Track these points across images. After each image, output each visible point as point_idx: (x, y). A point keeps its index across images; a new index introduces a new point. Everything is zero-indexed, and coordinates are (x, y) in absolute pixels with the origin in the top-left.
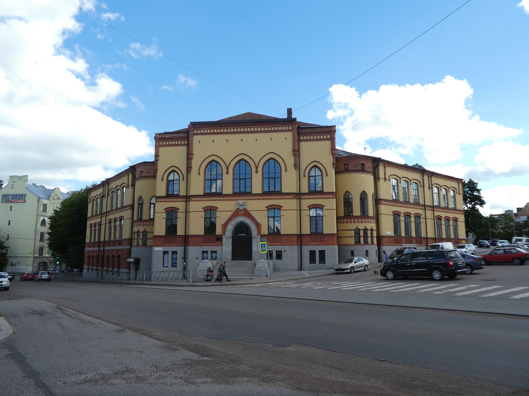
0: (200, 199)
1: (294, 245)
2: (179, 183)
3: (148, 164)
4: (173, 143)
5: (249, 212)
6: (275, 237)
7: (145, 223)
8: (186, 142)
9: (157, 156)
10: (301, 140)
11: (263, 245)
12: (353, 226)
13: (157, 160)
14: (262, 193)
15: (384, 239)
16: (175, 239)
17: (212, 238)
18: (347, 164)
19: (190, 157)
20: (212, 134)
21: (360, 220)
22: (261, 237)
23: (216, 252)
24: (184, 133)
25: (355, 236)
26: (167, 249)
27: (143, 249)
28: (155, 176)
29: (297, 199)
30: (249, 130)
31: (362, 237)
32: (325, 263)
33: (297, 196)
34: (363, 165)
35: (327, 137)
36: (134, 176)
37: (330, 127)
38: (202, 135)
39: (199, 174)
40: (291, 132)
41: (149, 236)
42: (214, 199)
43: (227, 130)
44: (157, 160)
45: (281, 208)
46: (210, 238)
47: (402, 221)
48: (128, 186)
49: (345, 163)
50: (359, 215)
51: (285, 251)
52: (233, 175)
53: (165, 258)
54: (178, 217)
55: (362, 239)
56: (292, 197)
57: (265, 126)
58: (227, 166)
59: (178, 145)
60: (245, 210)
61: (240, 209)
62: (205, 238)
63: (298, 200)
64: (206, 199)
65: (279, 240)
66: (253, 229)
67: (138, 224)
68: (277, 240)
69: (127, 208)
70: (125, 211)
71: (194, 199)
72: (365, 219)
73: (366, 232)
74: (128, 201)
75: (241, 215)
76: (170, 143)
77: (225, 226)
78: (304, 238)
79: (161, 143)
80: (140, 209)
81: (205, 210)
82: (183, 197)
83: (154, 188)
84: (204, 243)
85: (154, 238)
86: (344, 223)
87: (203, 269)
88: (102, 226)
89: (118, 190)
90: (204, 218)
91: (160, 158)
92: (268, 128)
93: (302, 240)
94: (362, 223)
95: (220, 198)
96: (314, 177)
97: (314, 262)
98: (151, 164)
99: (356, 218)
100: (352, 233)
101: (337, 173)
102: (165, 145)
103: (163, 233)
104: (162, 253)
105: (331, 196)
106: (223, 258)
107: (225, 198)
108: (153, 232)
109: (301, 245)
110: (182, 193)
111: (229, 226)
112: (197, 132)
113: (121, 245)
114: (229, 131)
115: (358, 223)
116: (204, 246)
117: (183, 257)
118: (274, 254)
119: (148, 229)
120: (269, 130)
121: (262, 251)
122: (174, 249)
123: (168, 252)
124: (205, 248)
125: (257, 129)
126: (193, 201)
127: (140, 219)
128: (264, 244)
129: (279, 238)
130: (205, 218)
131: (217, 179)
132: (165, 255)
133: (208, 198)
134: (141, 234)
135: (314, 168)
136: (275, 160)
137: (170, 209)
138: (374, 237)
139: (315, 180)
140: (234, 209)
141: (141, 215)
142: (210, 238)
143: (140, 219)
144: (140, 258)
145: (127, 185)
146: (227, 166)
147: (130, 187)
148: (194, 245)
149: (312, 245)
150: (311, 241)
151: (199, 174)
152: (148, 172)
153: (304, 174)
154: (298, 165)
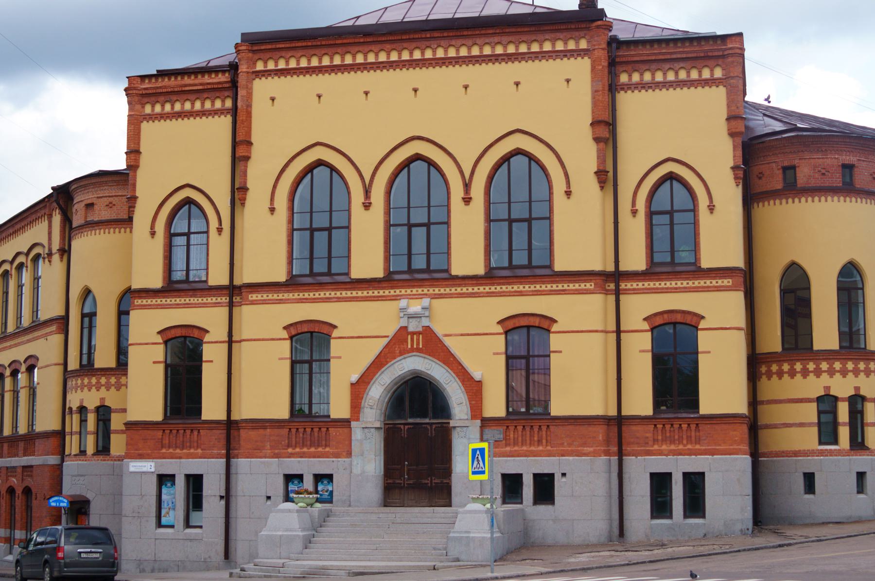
0: (275, 296)
1: (595, 454)
2: (208, 244)
3: (109, 178)
4: (188, 106)
5: (440, 341)
6: (532, 426)
7: (103, 380)
8: (229, 103)
9: (133, 152)
10: (623, 84)
11: (478, 452)
12: (814, 386)
13: (133, 168)
14: (486, 273)
15: (243, 433)
16: (196, 433)
17: (316, 430)
18: (793, 168)
19: (241, 152)
20: (314, 72)
21: (837, 365)
22: (482, 427)
23: (330, 477)
24: (224, 72)
25: (80, 432)
26: (168, 466)
27: (101, 465)
28: (128, 221)
29: (607, 292)
30: (440, 53)
31: (844, 424)
32: (703, 516)
33: (606, 281)
34: (848, 168)
35: (642, 79)
36: (67, 220)
37: (724, 38)
38: (282, 78)
39: (272, 210)
40: (586, 58)
41: (116, 422)
42: (322, 295)
43: (366, 58)
44: (133, 168)
45: (550, 326)
46: (309, 430)
47: (613, 332)
48: (50, 255)
49: (786, 164)
50: (836, 347)
51: (564, 475)
52: (388, 213)
53: (164, 497)
54: (552, 349)
55: (844, 433)
56: (588, 285)
57: (496, 39)
58: (367, 180)
59: (203, 113)
60: (428, 333)
61: (411, 329)
62: (294, 431)
63: (612, 298)
64: (296, 296)
65: (544, 436)
66: (453, 399)
67: (79, 382)
68: (536, 439)
69: (48, 330)
70: (42, 340)
71: (254, 297)
72: (804, 361)
73: (859, 407)
74: (50, 308)
75: (412, 350)
76: (178, 107)
77: (359, 389)
78: (629, 431)
79: (148, 109)
80: (86, 331)
81: (293, 333)
82: (218, 290)
83: (127, 265)
84: (289, 446)
85: (126, 430)
86: (780, 374)
87: (280, 533)
88: (28, 385)
89: (21, 266)
90: (503, 357)
91: (144, 160)
92: (505, 47)
93: (624, 435)
94: (844, 377)
95: (344, 293)
96: (668, 216)
97: (668, 514)
98: (115, 178)
99: (824, 360)
100: (810, 413)
101: (750, 200)
102: (149, 115)
103: (157, 415)
104: (154, 480)
105: (726, 281)
106: (352, 499)
107: (360, 294)
108: (124, 411)
109: (621, 454)
110: (218, 277)
111: (372, 389)
112: (276, 65)
113: (33, 454)
114: (371, 58)
115: (831, 377)
116: (290, 456)
117: (223, 494)
118: (528, 490)
119: (111, 399)
120: (346, 65)
121: (474, 473)
122: (194, 466)
123: (172, 478)
124: (294, 465)
125: (366, 59)
126: (253, 303)
127: (88, 368)
128: (482, 450)
129: (544, 428)
130: (293, 363)
131: (192, 230)
132: (163, 487)
133: (301, 294)
134: (91, 418)
135: (668, 184)
136: (531, 158)
137: (178, 332)
138: (87, 433)
139: (672, 224)
140: (391, 330)
141: (90, 354)
142: (309, 430)
143: (88, 368)
144: (89, 496)
145: (47, 251)
146: (367, 181)
147: (56, 258)
148: (254, 453)
149: (660, 453)
150: (658, 440)
151: (272, 210)
152: (110, 205)
153: (634, 203)
154: (611, 174)
